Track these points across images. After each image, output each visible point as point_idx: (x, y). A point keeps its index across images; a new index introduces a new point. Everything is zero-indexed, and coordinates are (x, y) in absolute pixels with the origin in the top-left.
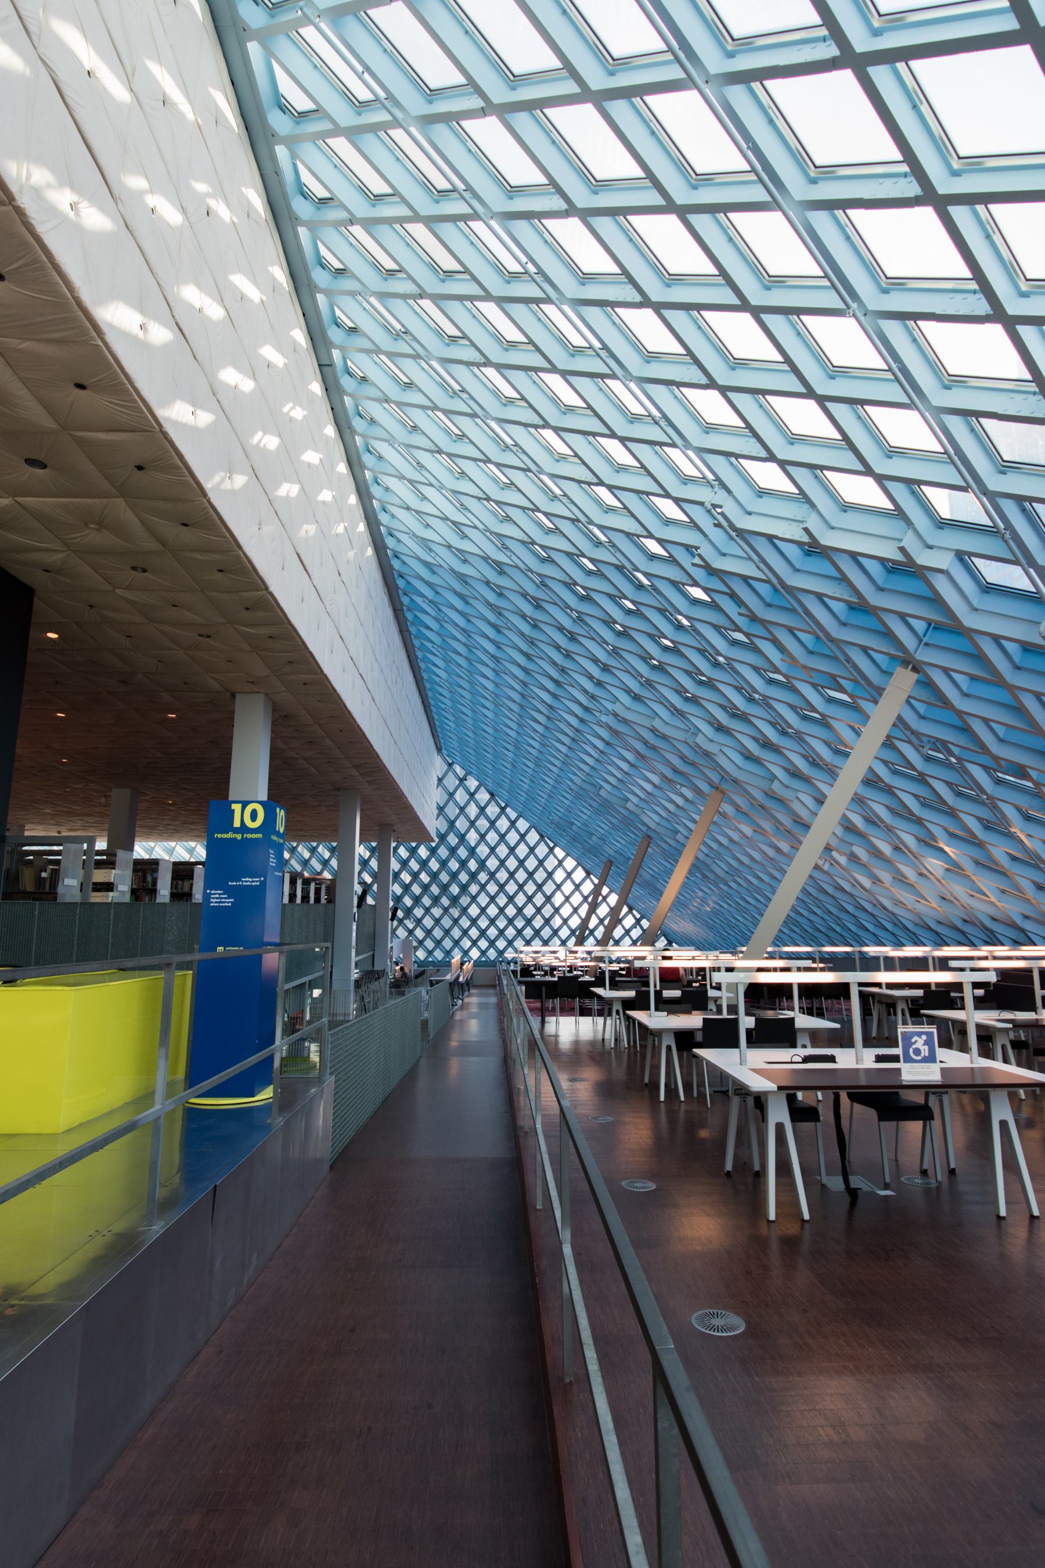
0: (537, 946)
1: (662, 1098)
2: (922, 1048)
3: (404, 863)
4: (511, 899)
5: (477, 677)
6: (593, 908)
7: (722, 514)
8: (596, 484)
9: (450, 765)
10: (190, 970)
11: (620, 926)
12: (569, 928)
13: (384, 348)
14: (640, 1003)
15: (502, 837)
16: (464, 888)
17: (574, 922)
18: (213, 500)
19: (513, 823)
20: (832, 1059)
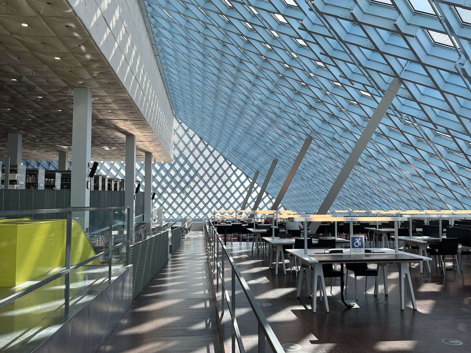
0: (223, 210)
1: (277, 273)
3: (158, 172)
4: (210, 189)
5: (194, 80)
7: (313, 4)
8: (299, 39)
9: (206, 146)
11: (262, 203)
14: (269, 234)
16: (187, 184)
17: (241, 200)
19: (234, 172)
20: (341, 252)
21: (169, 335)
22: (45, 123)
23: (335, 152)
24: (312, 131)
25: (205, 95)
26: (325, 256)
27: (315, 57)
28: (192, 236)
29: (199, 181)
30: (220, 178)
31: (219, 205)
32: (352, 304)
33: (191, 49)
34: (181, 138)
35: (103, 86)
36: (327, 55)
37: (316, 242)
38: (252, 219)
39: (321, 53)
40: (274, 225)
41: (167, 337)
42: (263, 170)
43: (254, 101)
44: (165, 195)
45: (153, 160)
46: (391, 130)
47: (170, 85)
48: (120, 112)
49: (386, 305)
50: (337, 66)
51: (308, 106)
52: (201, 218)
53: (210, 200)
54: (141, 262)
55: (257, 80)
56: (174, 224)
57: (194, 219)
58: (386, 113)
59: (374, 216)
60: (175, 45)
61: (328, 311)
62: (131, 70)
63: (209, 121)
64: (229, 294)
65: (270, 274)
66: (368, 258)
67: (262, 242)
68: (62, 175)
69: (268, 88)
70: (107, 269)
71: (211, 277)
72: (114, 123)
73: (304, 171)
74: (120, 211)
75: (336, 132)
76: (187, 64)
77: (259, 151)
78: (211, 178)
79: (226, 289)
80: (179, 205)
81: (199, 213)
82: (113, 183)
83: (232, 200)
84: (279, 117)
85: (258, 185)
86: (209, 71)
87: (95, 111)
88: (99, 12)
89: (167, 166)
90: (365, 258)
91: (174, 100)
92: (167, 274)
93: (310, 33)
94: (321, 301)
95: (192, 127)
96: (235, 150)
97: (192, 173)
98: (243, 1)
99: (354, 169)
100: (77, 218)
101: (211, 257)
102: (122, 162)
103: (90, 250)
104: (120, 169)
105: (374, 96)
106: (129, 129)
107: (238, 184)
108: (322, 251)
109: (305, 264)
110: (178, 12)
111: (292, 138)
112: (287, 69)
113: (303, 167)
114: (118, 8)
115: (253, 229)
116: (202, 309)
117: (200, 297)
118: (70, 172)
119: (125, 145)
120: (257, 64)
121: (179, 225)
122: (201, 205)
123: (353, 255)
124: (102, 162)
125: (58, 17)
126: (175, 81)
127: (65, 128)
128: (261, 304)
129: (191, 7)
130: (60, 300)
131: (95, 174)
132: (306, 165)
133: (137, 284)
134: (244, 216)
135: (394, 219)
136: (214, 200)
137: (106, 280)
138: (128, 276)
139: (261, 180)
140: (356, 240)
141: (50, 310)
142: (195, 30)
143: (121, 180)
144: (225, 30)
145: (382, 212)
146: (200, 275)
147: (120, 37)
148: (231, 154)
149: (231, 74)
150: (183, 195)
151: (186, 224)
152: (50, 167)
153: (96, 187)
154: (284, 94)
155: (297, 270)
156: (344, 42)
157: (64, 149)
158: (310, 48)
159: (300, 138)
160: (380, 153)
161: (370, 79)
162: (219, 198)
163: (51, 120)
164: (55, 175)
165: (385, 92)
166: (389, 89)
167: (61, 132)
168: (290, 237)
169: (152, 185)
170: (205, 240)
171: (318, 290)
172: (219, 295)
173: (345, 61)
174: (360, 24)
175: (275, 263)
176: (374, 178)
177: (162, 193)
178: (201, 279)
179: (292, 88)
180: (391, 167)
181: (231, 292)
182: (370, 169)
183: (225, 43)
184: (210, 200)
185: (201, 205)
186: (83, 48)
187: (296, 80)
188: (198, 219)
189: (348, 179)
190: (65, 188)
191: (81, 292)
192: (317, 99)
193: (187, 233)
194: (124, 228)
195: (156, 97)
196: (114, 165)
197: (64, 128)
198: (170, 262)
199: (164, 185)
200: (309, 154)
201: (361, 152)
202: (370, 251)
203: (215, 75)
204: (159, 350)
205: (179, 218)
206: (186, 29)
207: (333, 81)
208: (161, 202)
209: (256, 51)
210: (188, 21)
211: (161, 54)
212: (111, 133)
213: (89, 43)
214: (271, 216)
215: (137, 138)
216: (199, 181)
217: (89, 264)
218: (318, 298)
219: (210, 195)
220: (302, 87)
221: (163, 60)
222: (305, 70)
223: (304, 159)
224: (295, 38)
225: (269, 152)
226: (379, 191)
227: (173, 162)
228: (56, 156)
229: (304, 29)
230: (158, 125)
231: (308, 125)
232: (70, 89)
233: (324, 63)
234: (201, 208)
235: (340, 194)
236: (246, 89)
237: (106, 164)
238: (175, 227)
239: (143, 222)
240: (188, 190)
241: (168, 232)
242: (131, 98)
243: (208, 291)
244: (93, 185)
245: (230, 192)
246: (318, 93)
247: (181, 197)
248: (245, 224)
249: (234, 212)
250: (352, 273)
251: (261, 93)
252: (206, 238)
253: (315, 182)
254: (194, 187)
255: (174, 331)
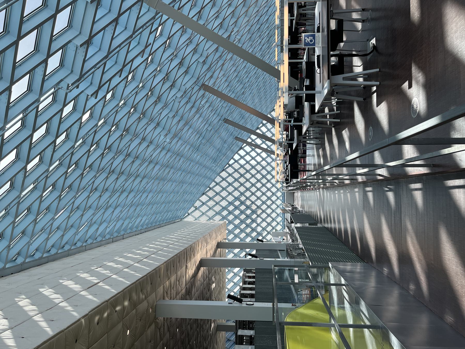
1: (339, 120)
2: (310, 39)
3: (236, 236)
4: (253, 185)
6: (258, 147)
7: (72, 84)
8: (106, 98)
9: (210, 189)
10: (284, 326)
11: (266, 133)
12: (267, 157)
13: (7, 243)
14: (300, 128)
15: (224, 189)
16: (248, 207)
17: (264, 155)
18: (65, 328)
19: (236, 161)
20: (318, 57)
21: (400, 228)
22: (190, 344)
23: (216, 61)
24: (196, 84)
25: (161, 190)
26: (323, 73)
27: (124, 82)
28: (300, 203)
29: (245, 196)
30: (242, 176)
31: (269, 177)
32: (371, 45)
33: (116, 205)
34: (203, 214)
35: (154, 289)
36: (121, 71)
37: (308, 81)
38: (283, 144)
39: (120, 77)
40: (289, 123)
41: (402, 229)
42: (235, 133)
43: (167, 142)
44: (259, 229)
45: (224, 241)
46: (195, 5)
47: (152, 224)
48: (179, 273)
49: (373, 10)
50: (132, 60)
51: (171, 88)
52: (281, 194)
53: (264, 185)
54: (326, 254)
55: (146, 139)
56: (287, 220)
57: (282, 200)
58: (178, 10)
59: (282, 21)
60: (113, 220)
61: (378, 70)
62: (137, 263)
63: (186, 186)
64: (360, 170)
65: (339, 128)
66: (326, 30)
67: (306, 134)
68: (240, 328)
69: (154, 129)
70: (333, 288)
71: (342, 185)
72: (190, 279)
73: (236, 91)
74: (276, 273)
75: (197, 60)
76: (132, 208)
77: (216, 138)
78: (242, 185)
79: (355, 172)
80: (269, 215)
81: (276, 196)
82: (247, 280)
83: (264, 163)
84: (182, 117)
85: (249, 138)
86: (138, 186)
87: (178, 297)
88: (83, 293)
89: (231, 227)
90: (326, 33)
91: (167, 220)
92: (338, 228)
93: (100, 88)
94: (367, 78)
95: (192, 203)
96: (215, 161)
97: (237, 203)
98: (70, 154)
99: (234, 41)
100: (283, 314)
101: (322, 186)
102: (227, 270)
103: (314, 303)
104: (233, 272)
105: (162, 22)
106: (195, 264)
107: (248, 158)
108: (317, 76)
109: (331, 93)
110: (81, 216)
111: (203, 104)
112: (135, 110)
113: (231, 93)
114: (78, 274)
115: (293, 143)
116: (374, 195)
117: (362, 197)
118: (237, 321)
119: (210, 268)
120: (131, 139)
121: (288, 216)
122: (269, 194)
123: (322, 45)
124: (227, 290)
125: (89, 332)
126: (148, 219)
127: (195, 325)
128: (370, 136)
129: (76, 204)
130: (365, 332)
131: (239, 297)
132: (230, 90)
133: (348, 258)
134: (280, 151)
135: (286, 4)
136: (264, 181)
137: (345, 288)
138: (341, 267)
139: (244, 135)
140: (307, 42)
141: (374, 343)
142: (98, 201)
143: (244, 272)
144: (98, 171)
145: (278, 13)
146: (339, 196)
147: (107, 273)
148: (218, 165)
149: (141, 165)
150: (259, 212)
151: (287, 209)
152: (232, 339)
153: (252, 296)
154: (159, 112)
155: (336, 100)
156: (109, 53)
157: (214, 326)
158: (114, 87)
159: (203, 96)
160: (218, 15)
161: (145, 27)
162: (262, 176)
163: (187, 338)
164: (240, 335)
165: (158, 12)
166: (154, 8)
167: (198, 330)
168: (303, 107)
169: (250, 241)
170: (304, 190)
171: (357, 80)
172: (360, 179)
173: (128, 52)
174: (91, 37)
175: (328, 122)
176: (243, 21)
177: (257, 232)
178: (343, 195)
179: (154, 105)
180: (232, 4)
181: (357, 168)
182: (234, 25)
183: (111, 171)
184: (264, 185)
185: (269, 194)
186: (118, 308)
187: (146, 100)
188: (282, 197)
189: (244, 47)
190: (253, 326)
191: (357, 313)
192: (165, 80)
193: (296, 208)
194: (292, 270)
195: (164, 238)
196: (229, 278)
197: (195, 326)
198: (326, 225)
199: (248, 230)
200: (219, 87)
201: (217, 34)
202: (319, 28)
203: (141, 181)
204: (414, 238)
205: (281, 215)
206: (98, 209)
207: (147, 64)
208: (266, 233)
209: (118, 141)
210: (90, 207)
211: (122, 233)
212: (199, 282)
213: (113, 303)
214: (282, 126)
215: (204, 256)
216: (245, 196)
217: (328, 303)
218: (365, 80)
219: (259, 185)
220: (153, 95)
221: (127, 231)
222: (137, 92)
223: (223, 92)
224: (105, 101)
225: (216, 127)
226: (256, 16)
227: (227, 221)
228: (221, 334)
229: (96, 93)
230: (190, 236)
231: (190, 89)
232: (157, 321)
233: (130, 73)
234: (272, 194)
235: (258, 55)
236: (155, 150)
237: (229, 287)
238: (291, 219)
239: (286, 251)
240: (254, 207)
241: (296, 228)
242: (165, 262)
243: (356, 188)
244: (249, 299)
245: (256, 165)
246: (159, 78)
247: (261, 213)
248: (288, 151)
249: (277, 162)
250: (340, 45)
251: (159, 135)
252: (302, 190)
253: (246, 81)
254: (251, 200)
255: (396, 223)
